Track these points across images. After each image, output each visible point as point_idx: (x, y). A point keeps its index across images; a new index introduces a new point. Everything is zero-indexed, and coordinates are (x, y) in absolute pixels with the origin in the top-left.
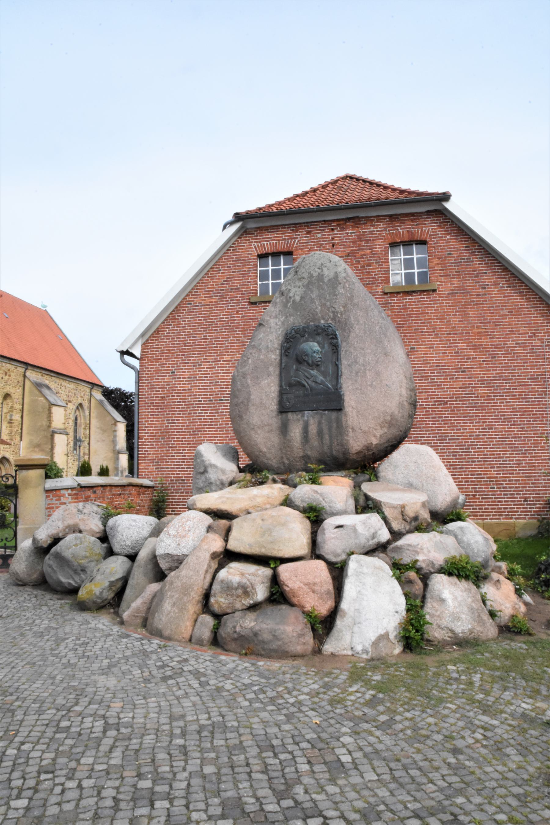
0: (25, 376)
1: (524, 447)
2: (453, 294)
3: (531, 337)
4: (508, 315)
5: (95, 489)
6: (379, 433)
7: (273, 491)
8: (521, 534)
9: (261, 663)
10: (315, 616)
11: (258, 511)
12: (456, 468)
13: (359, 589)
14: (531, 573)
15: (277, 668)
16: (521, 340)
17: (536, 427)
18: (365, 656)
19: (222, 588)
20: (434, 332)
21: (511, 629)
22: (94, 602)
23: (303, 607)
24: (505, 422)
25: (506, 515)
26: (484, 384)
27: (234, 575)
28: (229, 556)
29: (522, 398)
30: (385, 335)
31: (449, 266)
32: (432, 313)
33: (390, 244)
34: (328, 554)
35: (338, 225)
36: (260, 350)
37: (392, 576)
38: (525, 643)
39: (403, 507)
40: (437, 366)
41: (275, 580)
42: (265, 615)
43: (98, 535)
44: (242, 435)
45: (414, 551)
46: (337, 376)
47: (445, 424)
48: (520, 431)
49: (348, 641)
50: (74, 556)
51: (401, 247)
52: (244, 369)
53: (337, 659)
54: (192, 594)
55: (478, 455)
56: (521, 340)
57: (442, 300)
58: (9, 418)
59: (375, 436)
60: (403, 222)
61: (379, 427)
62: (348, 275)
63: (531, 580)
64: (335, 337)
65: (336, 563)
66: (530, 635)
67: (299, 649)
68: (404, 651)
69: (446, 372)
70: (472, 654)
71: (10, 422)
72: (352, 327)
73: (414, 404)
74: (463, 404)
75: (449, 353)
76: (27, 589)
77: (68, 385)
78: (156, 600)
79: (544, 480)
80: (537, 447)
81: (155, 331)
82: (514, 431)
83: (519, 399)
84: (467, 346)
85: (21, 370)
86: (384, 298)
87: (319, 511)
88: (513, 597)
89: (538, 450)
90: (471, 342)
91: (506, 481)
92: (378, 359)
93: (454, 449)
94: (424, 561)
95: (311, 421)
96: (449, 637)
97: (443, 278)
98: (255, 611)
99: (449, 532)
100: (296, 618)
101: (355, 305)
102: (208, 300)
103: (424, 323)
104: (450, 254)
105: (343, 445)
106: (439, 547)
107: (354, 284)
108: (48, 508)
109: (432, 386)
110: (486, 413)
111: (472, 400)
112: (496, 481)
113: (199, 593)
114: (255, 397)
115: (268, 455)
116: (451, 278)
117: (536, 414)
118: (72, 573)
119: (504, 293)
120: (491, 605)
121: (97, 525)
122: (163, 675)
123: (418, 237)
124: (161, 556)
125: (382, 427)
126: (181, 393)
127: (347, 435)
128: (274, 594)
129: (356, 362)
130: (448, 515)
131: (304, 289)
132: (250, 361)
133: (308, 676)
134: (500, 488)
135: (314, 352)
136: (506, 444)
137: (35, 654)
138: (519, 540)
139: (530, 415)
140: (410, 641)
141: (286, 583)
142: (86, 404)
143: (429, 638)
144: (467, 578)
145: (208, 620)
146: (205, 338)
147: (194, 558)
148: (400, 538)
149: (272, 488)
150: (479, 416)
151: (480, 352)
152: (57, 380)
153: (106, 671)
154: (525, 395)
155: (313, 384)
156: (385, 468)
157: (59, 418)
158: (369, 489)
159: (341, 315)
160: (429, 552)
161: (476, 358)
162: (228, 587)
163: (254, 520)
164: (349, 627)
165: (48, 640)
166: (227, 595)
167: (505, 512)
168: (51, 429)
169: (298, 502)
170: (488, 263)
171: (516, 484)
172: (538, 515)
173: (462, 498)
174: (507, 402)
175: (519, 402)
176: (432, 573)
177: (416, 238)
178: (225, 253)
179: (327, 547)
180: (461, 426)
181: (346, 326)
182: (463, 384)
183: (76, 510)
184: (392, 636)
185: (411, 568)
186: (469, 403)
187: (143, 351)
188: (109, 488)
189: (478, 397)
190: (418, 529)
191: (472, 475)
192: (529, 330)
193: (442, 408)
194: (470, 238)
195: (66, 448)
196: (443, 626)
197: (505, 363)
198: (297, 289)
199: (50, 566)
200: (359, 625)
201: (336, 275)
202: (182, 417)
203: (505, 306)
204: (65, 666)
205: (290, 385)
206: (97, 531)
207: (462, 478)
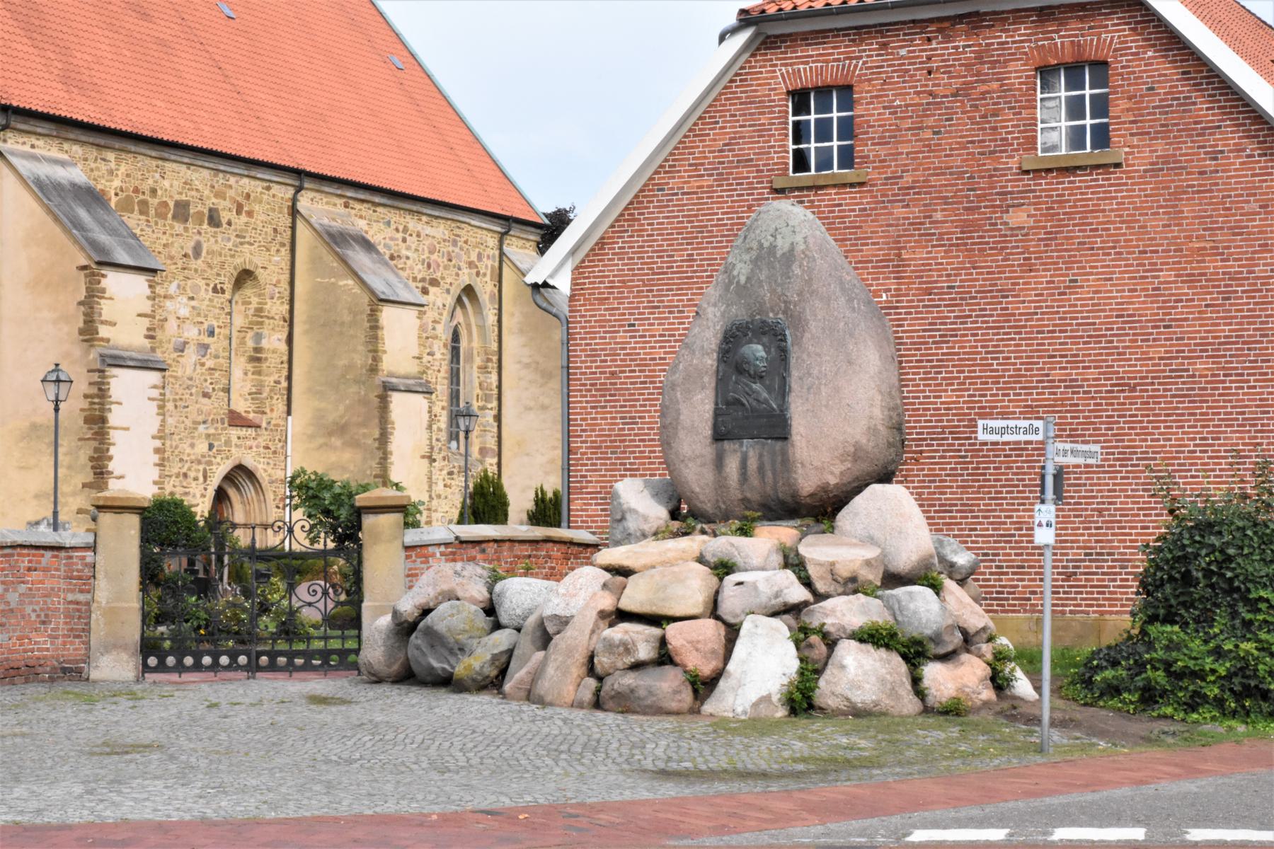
0: (294, 212)
2: (1154, 172)
4: (1259, 213)
5: (484, 545)
6: (838, 468)
12: (1150, 515)
18: (743, 717)
20: (1114, 248)
22: (474, 680)
24: (1244, 426)
26: (1207, 351)
28: (623, 616)
30: (852, 335)
31: (1149, 114)
32: (1112, 210)
35: (939, 31)
39: (833, 564)
40: (1117, 316)
41: (663, 642)
42: (653, 672)
46: (783, 392)
47: (1129, 428)
50: (449, 630)
57: (1133, 184)
58: (250, 344)
59: (832, 473)
60: (1062, 23)
67: (674, 705)
68: (789, 715)
69: (1135, 328)
71: (256, 358)
74: (1165, 390)
75: (1143, 290)
77: (428, 230)
81: (597, 244)
84: (1176, 276)
86: (1023, 180)
90: (1186, 269)
94: (833, 625)
95: (751, 453)
97: (1135, 139)
100: (676, 676)
102: (695, 183)
103: (1097, 230)
104: (1152, 89)
105: (790, 484)
106: (864, 610)
108: (408, 576)
109: (1107, 354)
110: (1208, 407)
111: (1183, 383)
115: (701, 497)
116: (1151, 139)
118: (446, 653)
119: (1254, 169)
125: (842, 462)
126: (645, 365)
129: (810, 374)
132: (681, 367)
142: (485, 289)
145: (592, 683)
146: (690, 259)
150: (1195, 414)
151: (1201, 287)
152: (395, 217)
155: (754, 403)
156: (845, 518)
157: (403, 340)
161: (1193, 300)
163: (652, 576)
168: (381, 377)
169: (709, 557)
170: (1225, 107)
174: (1249, 387)
177: (1086, 57)
178: (726, 88)
180: (1160, 434)
181: (799, 323)
186: (1177, 389)
188: (507, 544)
189: (1193, 376)
193: (1125, 398)
197: (1249, 310)
198: (742, 265)
199: (418, 648)
201: (792, 250)
202: (649, 411)
203: (1255, 195)
205: (728, 404)
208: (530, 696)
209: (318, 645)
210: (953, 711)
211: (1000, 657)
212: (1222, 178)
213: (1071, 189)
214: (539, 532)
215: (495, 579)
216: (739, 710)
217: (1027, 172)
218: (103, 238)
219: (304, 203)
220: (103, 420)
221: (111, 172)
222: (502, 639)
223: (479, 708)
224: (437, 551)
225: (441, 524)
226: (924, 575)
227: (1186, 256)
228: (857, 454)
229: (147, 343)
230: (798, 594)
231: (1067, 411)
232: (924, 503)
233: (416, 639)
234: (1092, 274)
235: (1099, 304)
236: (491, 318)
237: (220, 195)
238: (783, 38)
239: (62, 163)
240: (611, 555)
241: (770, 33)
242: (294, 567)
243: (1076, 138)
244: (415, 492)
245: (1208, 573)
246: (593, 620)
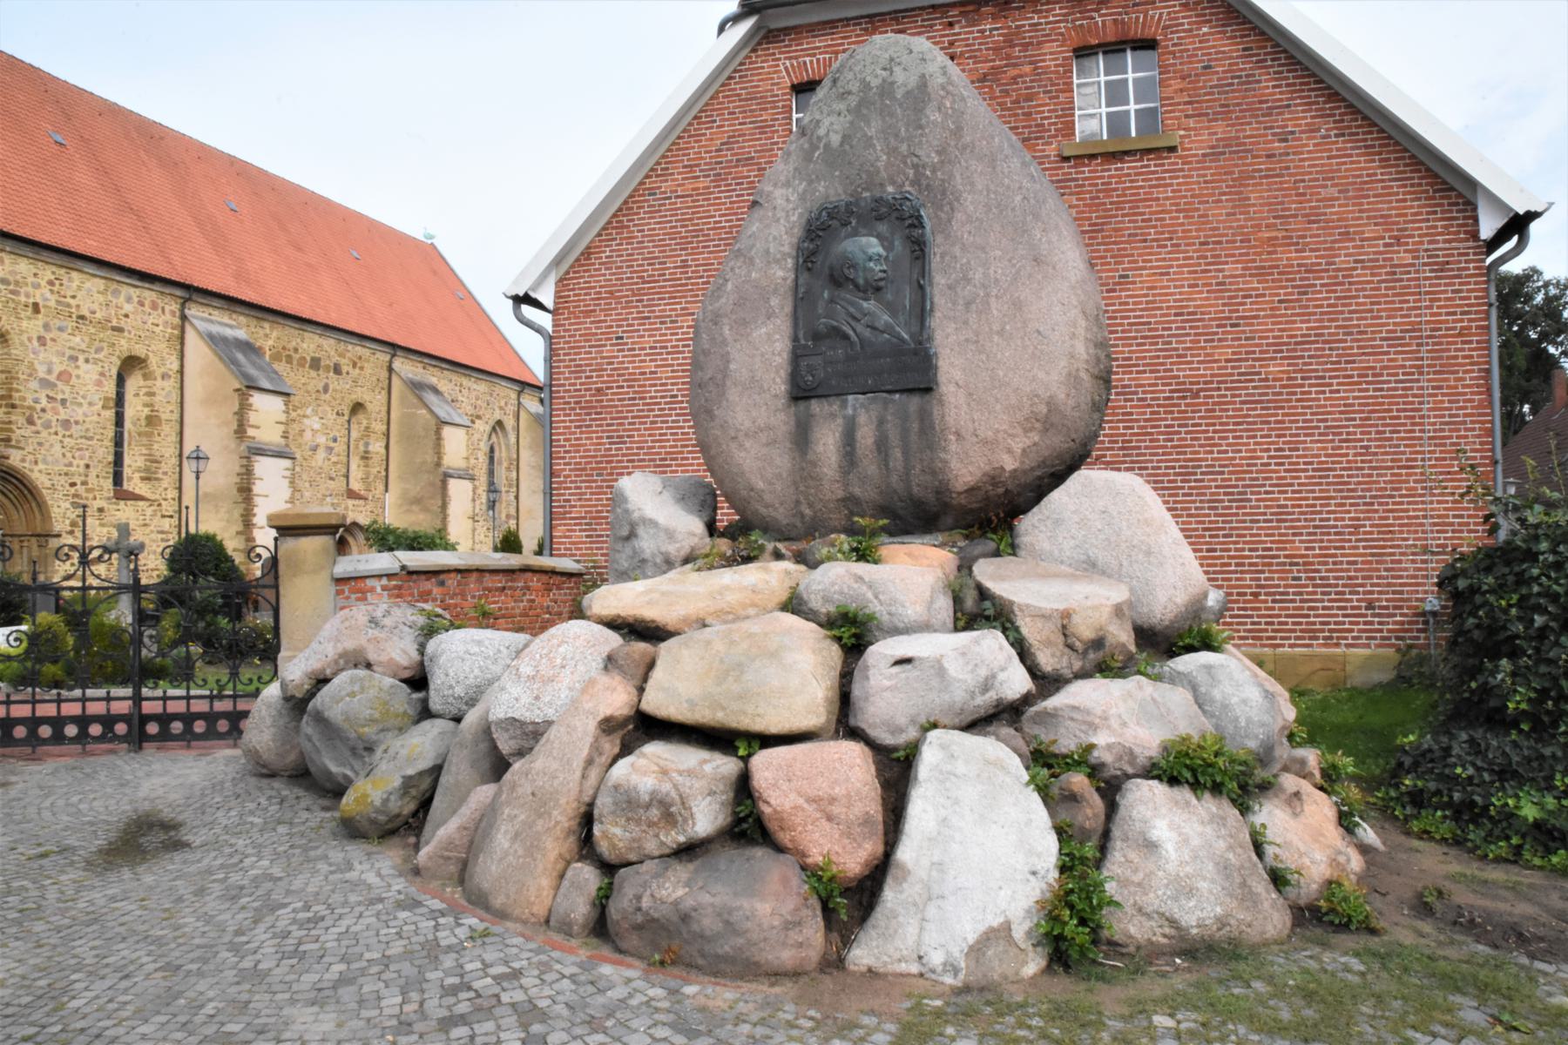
0: (390, 370)
1: (1370, 490)
2: (1215, 155)
3: (1390, 245)
4: (1338, 199)
5: (442, 577)
6: (1018, 445)
7: (770, 576)
8: (1358, 680)
9: (690, 990)
10: (832, 879)
11: (726, 622)
12: (1217, 536)
13: (943, 813)
14: (1377, 772)
15: (725, 1006)
16: (1367, 254)
17: (1398, 446)
18: (948, 980)
19: (616, 804)
21: (1322, 917)
22: (373, 822)
23: (804, 855)
25: (1325, 638)
27: (645, 774)
28: (647, 727)
29: (1367, 383)
30: (1037, 217)
32: (1167, 198)
33: (1075, 50)
34: (874, 726)
35: (962, 14)
36: (751, 259)
37: (1028, 784)
38: (1357, 955)
39: (1066, 615)
41: (743, 787)
43: (407, 674)
44: (713, 452)
45: (1084, 722)
46: (921, 311)
48: (1361, 454)
49: (911, 941)
50: (347, 719)
51: (1101, 57)
52: (717, 305)
53: (879, 984)
54: (555, 813)
55: (1266, 507)
56: (1367, 254)
58: (362, 448)
59: (1010, 451)
61: (1019, 431)
62: (950, 82)
63: (1378, 790)
64: (918, 223)
65: (895, 749)
66: (1373, 932)
68: (1048, 970)
70: (1220, 982)
71: (366, 457)
72: (957, 199)
73: (1104, 379)
74: (1233, 396)
75: (1205, 285)
76: (277, 784)
78: (483, 824)
79: (1413, 561)
80: (1399, 489)
82: (1347, 455)
83: (1360, 383)
87: (864, 624)
88: (1333, 834)
89: (1401, 496)
90: (1254, 261)
91: (1326, 563)
92: (1018, 272)
93: (1212, 494)
94: (1109, 747)
95: (862, 418)
96: (1165, 936)
98: (691, 861)
99: (1175, 679)
100: (785, 881)
101: (965, 148)
107: (963, 99)
109: (1165, 357)
111: (1255, 388)
112: (1305, 564)
113: (571, 813)
114: (739, 365)
115: (768, 497)
117: (1398, 418)
120: (1276, 856)
121: (405, 652)
122: (446, 1013)
123: (1137, 32)
124: (500, 722)
125: (1026, 431)
127: (944, 450)
128: (743, 820)
129: (968, 281)
130: (1181, 637)
131: (849, 118)
132: (729, 286)
133: (795, 1032)
134: (1313, 579)
135: (870, 259)
136: (1328, 484)
137: (197, 941)
138: (1356, 692)
139: (1384, 418)
140: (1063, 946)
141: (765, 795)
142: (509, 423)
143: (1116, 938)
144: (1217, 789)
145: (587, 876)
147: (562, 729)
148: (1058, 690)
149: (766, 570)
152: (454, 377)
153: (327, 993)
154: (1374, 375)
155: (867, 333)
156: (1032, 526)
157: (456, 447)
158: (988, 572)
159: (934, 171)
160: (1124, 724)
161: (1264, 295)
162: (629, 802)
163: (708, 643)
164: (915, 904)
165: (243, 908)
166: (628, 819)
167: (1323, 631)
168: (442, 469)
169: (816, 603)
170: (1294, 84)
171: (1348, 570)
172: (1397, 638)
173: (1214, 598)
175: (1360, 390)
176: (1128, 777)
178: (723, 85)
179: (871, 709)
181: (944, 197)
182: (1234, 353)
183: (366, 618)
184: (1019, 933)
185: (1078, 763)
187: (558, 295)
188: (474, 576)
189: (1267, 380)
190: (1105, 669)
191: (1251, 550)
192: (1385, 230)
194: (1253, 29)
195: (470, 505)
196: (1149, 909)
198: (833, 118)
200: (939, 902)
201: (923, 83)
204: (243, 976)
205: (817, 337)
206: (405, 663)
207: (1230, 557)
212: (1292, 161)
213: (1119, 176)
215: (429, 632)
216: (936, 959)
217: (1067, 159)
218: (253, 372)
219: (398, 364)
220: (250, 490)
221: (266, 335)
224: (377, 584)
227: (1255, 247)
229: (283, 441)
231: (1119, 421)
234: (1144, 268)
235: (1154, 302)
236: (513, 440)
237: (341, 355)
238: (786, 31)
239: (231, 327)
241: (773, 26)
246: (589, 739)
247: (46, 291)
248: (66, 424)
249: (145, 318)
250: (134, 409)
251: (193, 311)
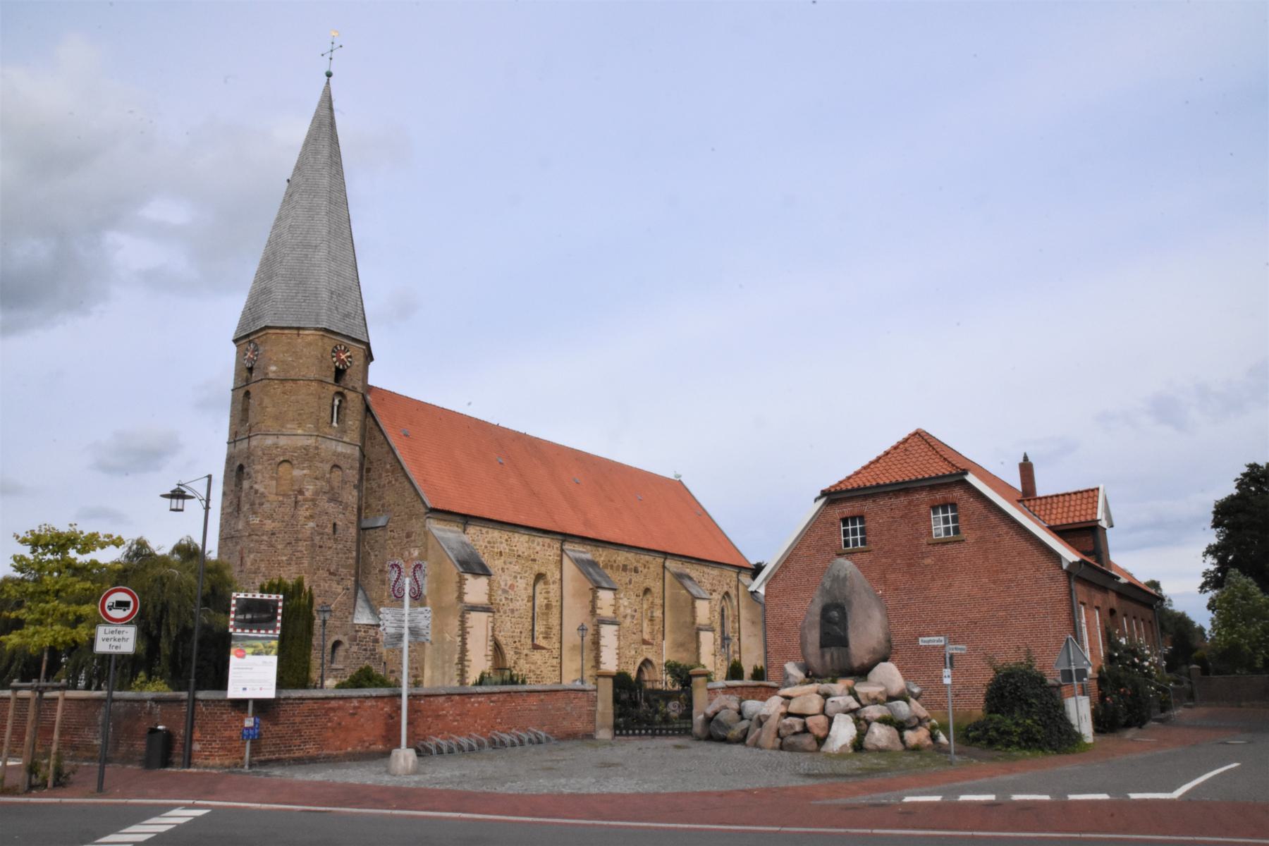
0: (664, 567)
28: (789, 714)
41: (805, 724)
42: (801, 737)
46: (845, 629)
71: (652, 620)
85: (660, 560)
106: (880, 710)
142: (733, 592)
156: (871, 676)
157: (703, 611)
208: (756, 745)
209: (677, 726)
210: (916, 749)
211: (933, 728)
214: (756, 683)
215: (741, 701)
218: (598, 578)
219: (668, 563)
222: (745, 724)
223: (737, 749)
225: (720, 681)
226: (903, 697)
228: (874, 651)
230: (855, 705)
232: (900, 669)
233: (712, 724)
240: (786, 691)
242: (667, 696)
243: (947, 531)
244: (710, 668)
245: (1010, 693)
247: (504, 545)
248: (512, 611)
249: (545, 550)
250: (540, 600)
251: (567, 546)
